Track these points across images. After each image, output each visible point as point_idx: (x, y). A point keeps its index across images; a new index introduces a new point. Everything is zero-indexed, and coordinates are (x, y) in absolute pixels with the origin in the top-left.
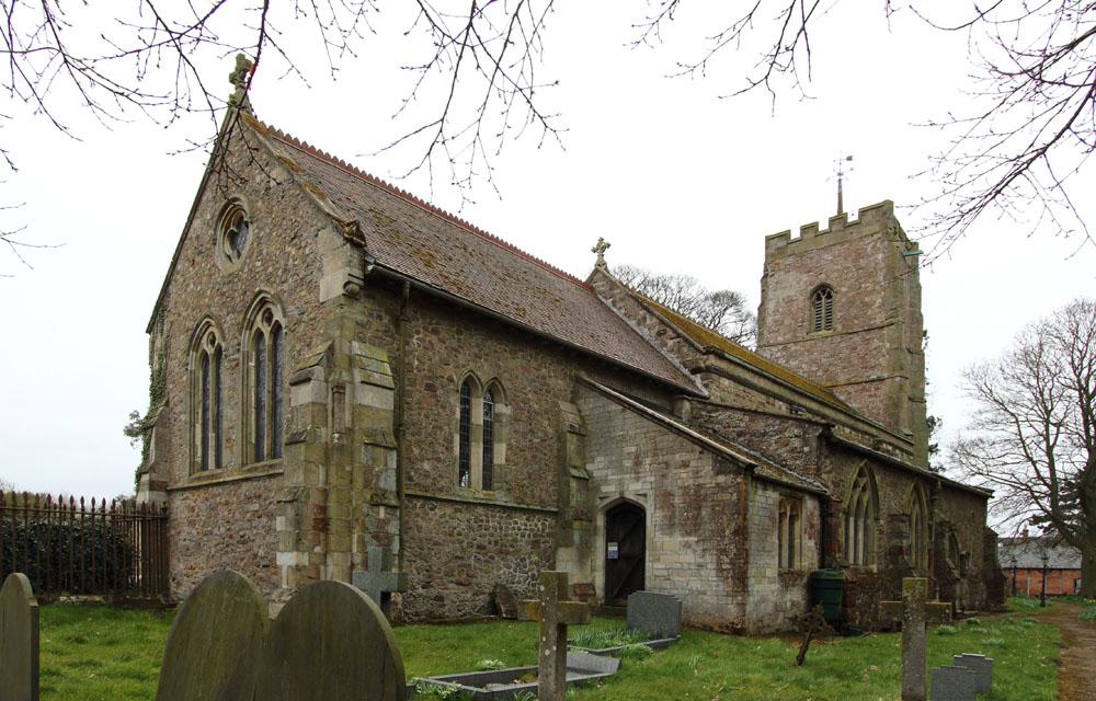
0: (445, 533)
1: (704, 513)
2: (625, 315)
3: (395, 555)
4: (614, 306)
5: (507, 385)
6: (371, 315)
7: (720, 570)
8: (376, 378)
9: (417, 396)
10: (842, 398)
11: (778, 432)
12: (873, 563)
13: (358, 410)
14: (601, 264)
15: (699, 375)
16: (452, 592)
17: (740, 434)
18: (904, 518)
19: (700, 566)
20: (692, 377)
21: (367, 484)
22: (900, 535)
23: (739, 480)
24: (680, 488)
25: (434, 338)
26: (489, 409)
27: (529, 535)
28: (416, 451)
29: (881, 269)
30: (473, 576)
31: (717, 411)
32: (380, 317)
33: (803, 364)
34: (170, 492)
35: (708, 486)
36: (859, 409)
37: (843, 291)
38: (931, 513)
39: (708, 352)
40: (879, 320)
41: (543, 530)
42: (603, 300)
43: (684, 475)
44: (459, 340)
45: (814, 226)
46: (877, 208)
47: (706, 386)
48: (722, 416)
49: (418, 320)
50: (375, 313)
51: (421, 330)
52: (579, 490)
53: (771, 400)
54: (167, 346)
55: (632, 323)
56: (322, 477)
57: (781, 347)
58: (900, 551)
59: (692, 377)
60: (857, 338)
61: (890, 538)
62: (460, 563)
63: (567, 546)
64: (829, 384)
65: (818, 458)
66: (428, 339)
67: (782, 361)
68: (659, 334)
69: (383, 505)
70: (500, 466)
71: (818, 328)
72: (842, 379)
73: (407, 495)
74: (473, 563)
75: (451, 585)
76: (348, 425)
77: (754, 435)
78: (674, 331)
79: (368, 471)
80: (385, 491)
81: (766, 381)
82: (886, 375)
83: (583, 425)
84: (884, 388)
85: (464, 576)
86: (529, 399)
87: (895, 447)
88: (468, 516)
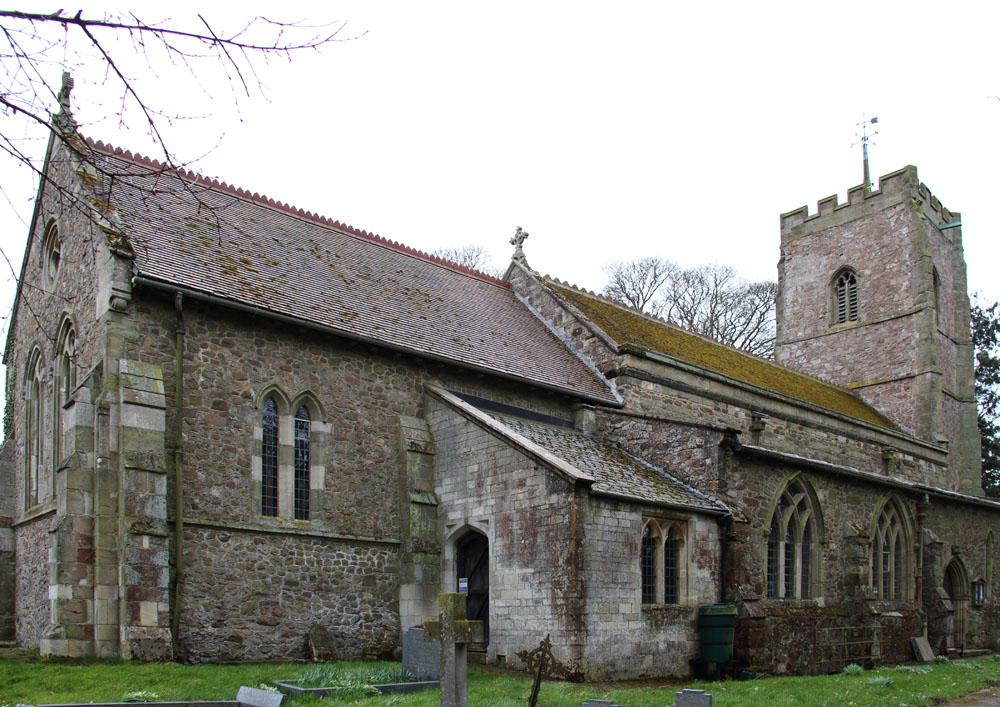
0: (240, 566)
1: (539, 540)
2: (542, 313)
3: (164, 589)
4: (531, 304)
5: (323, 399)
6: (144, 330)
7: (555, 606)
8: (144, 397)
9: (202, 415)
10: (869, 401)
11: (681, 442)
12: (819, 596)
13: (123, 432)
14: (519, 257)
15: (614, 380)
16: (253, 632)
17: (644, 447)
18: (861, 540)
19: (537, 602)
20: (608, 382)
21: (129, 511)
22: (856, 560)
23: (570, 499)
24: (518, 511)
25: (226, 352)
26: (300, 427)
27: (360, 571)
28: (202, 476)
29: (906, 246)
30: (281, 616)
31: (622, 420)
32: (156, 332)
33: (824, 364)
34: (14, 528)
35: (542, 508)
36: (888, 413)
37: (866, 273)
38: (918, 533)
39: (622, 352)
40: (907, 306)
41: (380, 565)
42: (520, 298)
43: (521, 496)
44: (259, 352)
45: (832, 200)
46: (898, 174)
47: (621, 392)
48: (626, 425)
49: (205, 332)
50: (149, 328)
51: (210, 343)
52: (422, 518)
53: (722, 406)
54: (15, 375)
55: (548, 323)
56: (87, 505)
57: (801, 344)
58: (856, 580)
59: (608, 382)
60: (883, 329)
61: (845, 566)
62: (263, 599)
63: (408, 582)
64: (855, 385)
65: (722, 471)
66: (218, 352)
67: (803, 360)
68: (575, 334)
69: (147, 534)
70: (318, 491)
71: (842, 320)
72: (869, 379)
73: (185, 524)
74: (280, 601)
75: (251, 625)
76: (113, 448)
77: (656, 447)
78: (590, 330)
79: (131, 497)
80: (152, 519)
81: (713, 383)
82: (916, 372)
83: (431, 443)
84: (916, 387)
85: (270, 615)
86: (357, 415)
87: (917, 457)
88: (272, 548)
